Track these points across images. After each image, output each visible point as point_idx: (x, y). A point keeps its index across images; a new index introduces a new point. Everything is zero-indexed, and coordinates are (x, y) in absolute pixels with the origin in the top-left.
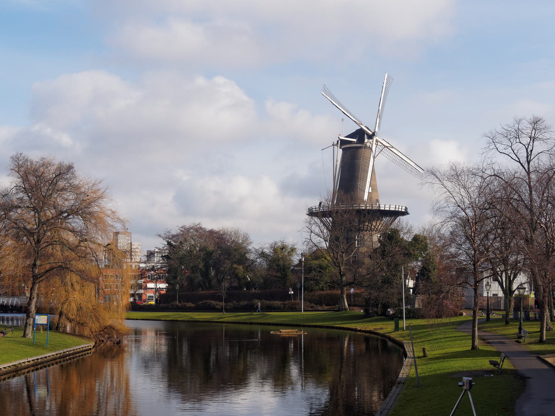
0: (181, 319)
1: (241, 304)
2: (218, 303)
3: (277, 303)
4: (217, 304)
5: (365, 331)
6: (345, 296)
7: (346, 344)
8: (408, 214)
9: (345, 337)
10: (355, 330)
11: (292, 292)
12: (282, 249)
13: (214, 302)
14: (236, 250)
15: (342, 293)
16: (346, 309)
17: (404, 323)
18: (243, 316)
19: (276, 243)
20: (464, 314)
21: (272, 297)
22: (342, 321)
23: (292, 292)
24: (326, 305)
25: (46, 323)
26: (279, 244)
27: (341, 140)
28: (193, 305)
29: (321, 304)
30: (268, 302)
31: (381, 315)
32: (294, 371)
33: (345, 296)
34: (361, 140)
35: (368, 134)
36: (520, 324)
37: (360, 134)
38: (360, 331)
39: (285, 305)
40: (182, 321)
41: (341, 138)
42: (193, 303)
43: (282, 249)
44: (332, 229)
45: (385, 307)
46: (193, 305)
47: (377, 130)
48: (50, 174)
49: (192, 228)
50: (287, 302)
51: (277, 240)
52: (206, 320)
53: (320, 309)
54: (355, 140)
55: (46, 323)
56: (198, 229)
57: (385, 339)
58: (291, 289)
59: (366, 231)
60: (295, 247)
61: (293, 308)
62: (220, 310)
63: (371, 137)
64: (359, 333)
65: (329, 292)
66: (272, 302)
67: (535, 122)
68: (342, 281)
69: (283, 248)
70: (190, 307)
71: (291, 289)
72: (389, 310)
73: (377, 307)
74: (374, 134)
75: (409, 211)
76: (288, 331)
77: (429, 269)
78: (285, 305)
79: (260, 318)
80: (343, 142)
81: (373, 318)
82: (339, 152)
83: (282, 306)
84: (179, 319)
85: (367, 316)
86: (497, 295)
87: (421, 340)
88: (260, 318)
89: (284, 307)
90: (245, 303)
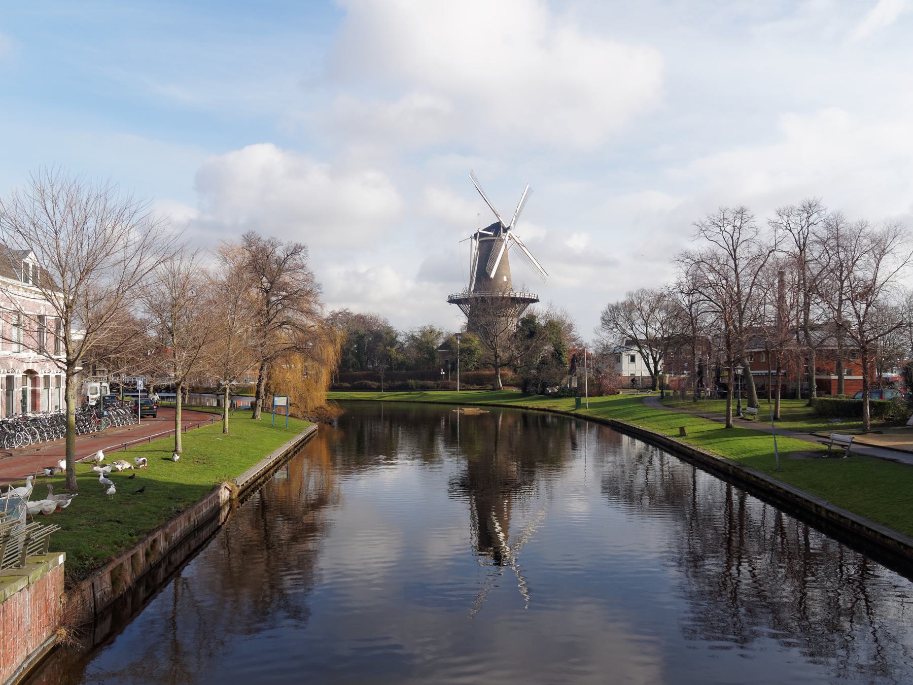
0: (343, 398)
1: (396, 384)
2: (373, 383)
3: (430, 383)
4: (373, 384)
5: (538, 409)
6: (499, 376)
7: (500, 420)
8: (538, 301)
9: (500, 413)
10: (526, 408)
11: (444, 373)
12: (431, 333)
13: (370, 382)
14: (387, 333)
15: (497, 373)
16: (500, 389)
17: (586, 400)
18: (403, 395)
19: (425, 327)
20: (621, 392)
21: (423, 377)
22: (503, 399)
23: (444, 373)
24: (477, 385)
25: (285, 404)
26: (428, 328)
27: (480, 233)
28: (348, 385)
29: (472, 384)
30: (422, 382)
31: (540, 394)
32: (441, 446)
33: (499, 376)
34: (497, 233)
35: (503, 228)
36: (739, 402)
37: (497, 228)
38: (532, 409)
39: (438, 385)
40: (345, 400)
41: (480, 231)
42: (349, 384)
43: (431, 333)
44: (471, 316)
45: (544, 386)
46: (348, 385)
47: (512, 225)
48: (280, 252)
49: (340, 313)
50: (439, 382)
51: (425, 324)
52: (368, 399)
53: (472, 388)
54: (492, 233)
55: (285, 404)
56: (346, 314)
57: (329, 409)
58: (442, 370)
59: (503, 317)
60: (442, 331)
61: (446, 388)
62: (378, 389)
63: (505, 230)
64: (530, 411)
65: (475, 372)
66: (426, 382)
67: (741, 211)
68: (496, 363)
69: (432, 331)
70: (347, 387)
71: (442, 370)
72: (548, 389)
73: (537, 386)
74: (509, 228)
75: (539, 298)
76: (470, 409)
77: (560, 351)
78: (438, 385)
79: (420, 397)
80: (482, 235)
81: (534, 397)
82: (476, 243)
83: (436, 386)
84: (341, 398)
85: (525, 394)
86: (634, 375)
87: (632, 418)
88: (420, 397)
89: (438, 387)
90: (400, 383)
